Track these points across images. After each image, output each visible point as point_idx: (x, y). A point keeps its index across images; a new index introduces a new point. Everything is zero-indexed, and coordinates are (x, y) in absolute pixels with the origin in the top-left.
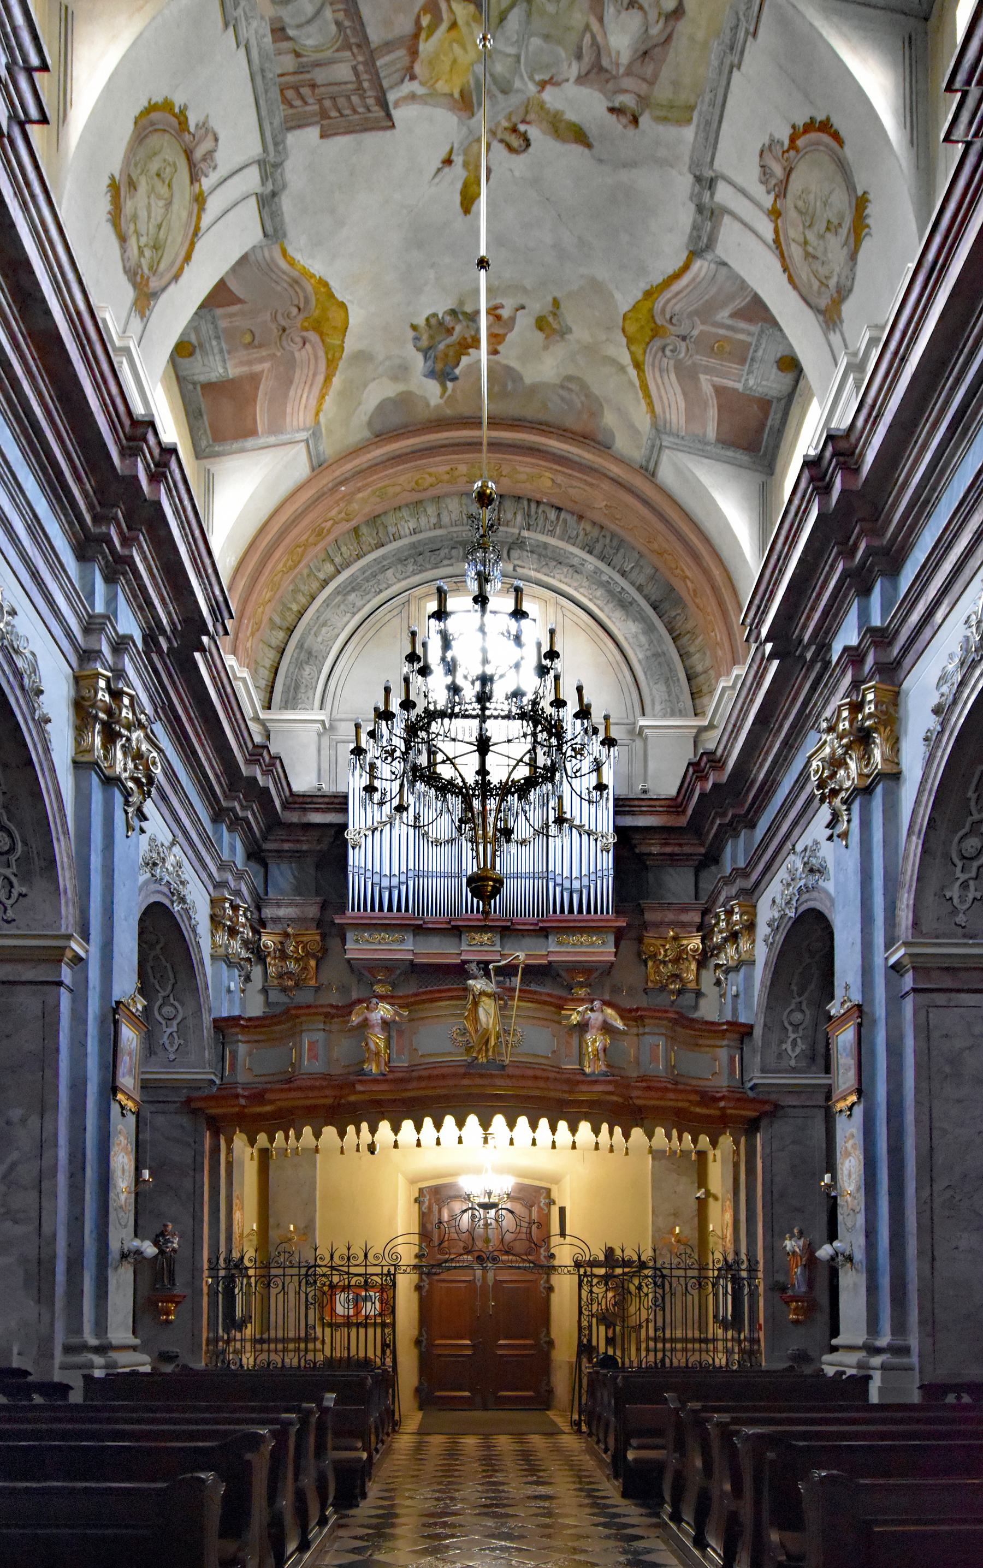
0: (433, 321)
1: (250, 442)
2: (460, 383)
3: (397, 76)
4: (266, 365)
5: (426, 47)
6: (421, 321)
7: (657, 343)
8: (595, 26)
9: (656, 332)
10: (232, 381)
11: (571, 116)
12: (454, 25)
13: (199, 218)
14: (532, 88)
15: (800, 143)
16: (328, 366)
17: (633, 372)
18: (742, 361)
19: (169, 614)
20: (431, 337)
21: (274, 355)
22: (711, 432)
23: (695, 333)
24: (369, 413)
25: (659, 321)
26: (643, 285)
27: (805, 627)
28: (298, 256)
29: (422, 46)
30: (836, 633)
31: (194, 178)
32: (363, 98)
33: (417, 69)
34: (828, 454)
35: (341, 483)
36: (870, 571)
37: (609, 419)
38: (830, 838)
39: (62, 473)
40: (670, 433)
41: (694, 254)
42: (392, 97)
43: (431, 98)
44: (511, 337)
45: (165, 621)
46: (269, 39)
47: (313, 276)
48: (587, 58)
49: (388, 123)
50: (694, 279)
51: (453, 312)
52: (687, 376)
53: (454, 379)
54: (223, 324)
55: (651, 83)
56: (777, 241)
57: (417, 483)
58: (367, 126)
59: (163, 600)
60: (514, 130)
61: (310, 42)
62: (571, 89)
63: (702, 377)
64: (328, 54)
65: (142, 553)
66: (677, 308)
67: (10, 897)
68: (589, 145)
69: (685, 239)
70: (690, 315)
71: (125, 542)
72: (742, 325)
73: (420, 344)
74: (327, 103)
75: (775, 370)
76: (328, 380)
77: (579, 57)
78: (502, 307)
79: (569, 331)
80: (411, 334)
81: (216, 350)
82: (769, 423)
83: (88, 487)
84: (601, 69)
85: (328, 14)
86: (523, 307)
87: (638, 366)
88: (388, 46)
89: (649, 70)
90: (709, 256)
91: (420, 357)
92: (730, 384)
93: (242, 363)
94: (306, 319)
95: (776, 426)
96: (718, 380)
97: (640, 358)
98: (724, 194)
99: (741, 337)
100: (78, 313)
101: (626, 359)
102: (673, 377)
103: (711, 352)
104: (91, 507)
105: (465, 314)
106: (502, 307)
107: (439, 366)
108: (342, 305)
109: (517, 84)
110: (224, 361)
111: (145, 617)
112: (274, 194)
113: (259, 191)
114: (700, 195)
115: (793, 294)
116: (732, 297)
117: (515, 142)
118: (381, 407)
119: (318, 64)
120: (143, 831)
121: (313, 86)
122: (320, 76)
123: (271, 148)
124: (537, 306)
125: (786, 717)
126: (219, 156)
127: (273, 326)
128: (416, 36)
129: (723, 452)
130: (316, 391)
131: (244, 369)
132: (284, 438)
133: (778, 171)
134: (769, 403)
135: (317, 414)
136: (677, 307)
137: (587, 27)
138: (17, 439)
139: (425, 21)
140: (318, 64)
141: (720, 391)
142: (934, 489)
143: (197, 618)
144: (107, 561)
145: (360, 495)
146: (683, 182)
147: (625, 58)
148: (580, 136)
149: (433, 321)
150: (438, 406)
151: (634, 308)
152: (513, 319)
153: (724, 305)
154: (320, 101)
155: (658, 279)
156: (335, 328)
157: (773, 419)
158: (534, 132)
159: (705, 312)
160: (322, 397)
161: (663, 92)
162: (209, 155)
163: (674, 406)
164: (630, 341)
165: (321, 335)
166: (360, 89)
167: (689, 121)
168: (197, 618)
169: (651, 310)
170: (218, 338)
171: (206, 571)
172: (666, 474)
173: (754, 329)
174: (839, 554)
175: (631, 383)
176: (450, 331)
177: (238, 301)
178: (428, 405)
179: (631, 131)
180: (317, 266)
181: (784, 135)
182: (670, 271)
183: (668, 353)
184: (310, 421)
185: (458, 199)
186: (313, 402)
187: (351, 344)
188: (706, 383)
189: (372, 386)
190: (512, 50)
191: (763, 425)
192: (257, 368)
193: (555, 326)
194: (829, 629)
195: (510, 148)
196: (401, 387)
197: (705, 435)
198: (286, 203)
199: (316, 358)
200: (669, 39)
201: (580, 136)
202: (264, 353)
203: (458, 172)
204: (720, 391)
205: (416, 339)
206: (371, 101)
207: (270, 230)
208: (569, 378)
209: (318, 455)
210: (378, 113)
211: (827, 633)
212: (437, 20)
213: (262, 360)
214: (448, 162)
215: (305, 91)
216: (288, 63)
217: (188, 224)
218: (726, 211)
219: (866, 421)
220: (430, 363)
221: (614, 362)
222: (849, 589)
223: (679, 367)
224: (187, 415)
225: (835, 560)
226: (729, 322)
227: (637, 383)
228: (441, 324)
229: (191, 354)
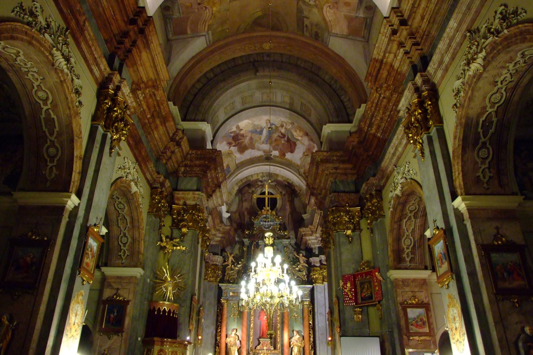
38: (415, 157)
67: (124, 256)
120: (119, 155)
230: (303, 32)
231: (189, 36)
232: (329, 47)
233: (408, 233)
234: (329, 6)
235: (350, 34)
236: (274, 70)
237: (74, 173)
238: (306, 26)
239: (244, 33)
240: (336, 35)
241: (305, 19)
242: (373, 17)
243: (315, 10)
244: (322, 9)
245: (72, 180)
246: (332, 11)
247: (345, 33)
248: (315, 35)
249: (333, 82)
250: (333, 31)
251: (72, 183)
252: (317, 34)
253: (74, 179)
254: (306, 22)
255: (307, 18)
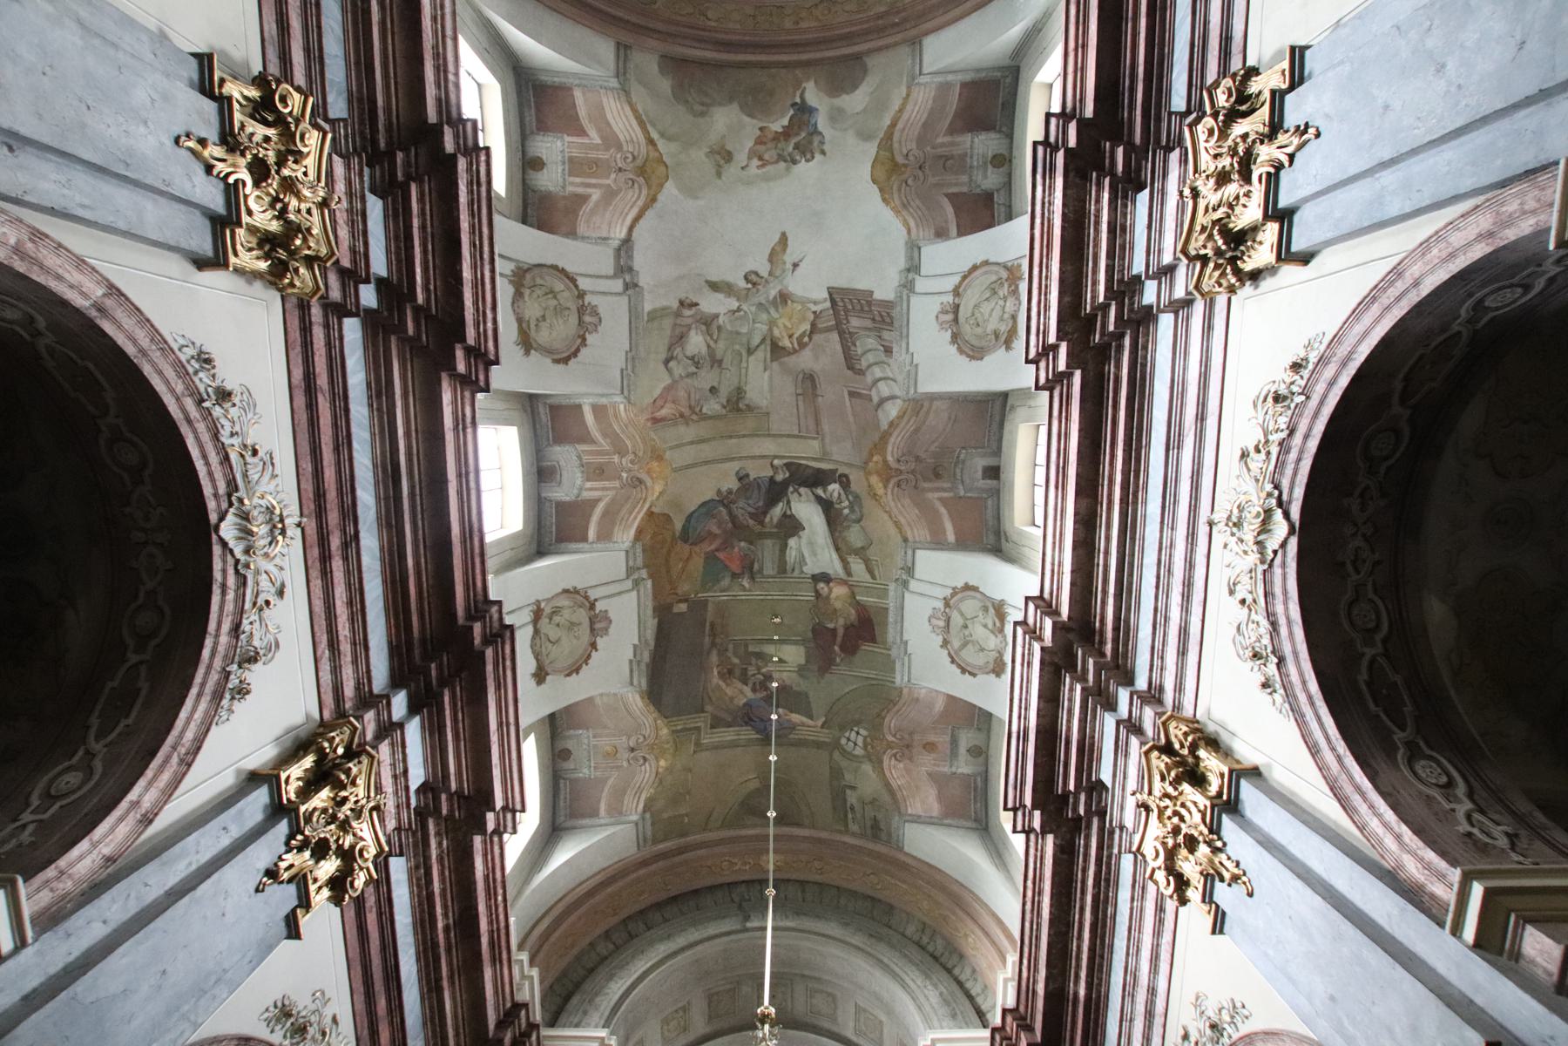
0: (808, 156)
1: (968, 77)
2: (790, 102)
3: (824, 314)
4: (940, 140)
5: (806, 327)
6: (818, 157)
7: (639, 162)
8: (712, 343)
9: (642, 171)
10: (970, 130)
11: (720, 296)
12: (790, 337)
13: (961, 283)
14: (745, 307)
15: (579, 341)
16: (892, 134)
17: (655, 135)
18: (571, 160)
19: (1098, 201)
20: (810, 143)
21: (933, 148)
22: (578, 94)
23: (613, 176)
24: (865, 83)
25: (641, 180)
26: (658, 205)
27: (421, 200)
28: (900, 226)
29: (808, 327)
30: (386, 216)
31: (956, 308)
32: (845, 306)
33: (812, 317)
34: (482, 377)
35: (897, 24)
36: (390, 310)
37: (665, 85)
39: (1128, 399)
40: (612, 89)
41: (627, 242)
42: (828, 304)
43: (804, 302)
44: (750, 144)
45: (1106, 196)
46: (894, 350)
47: (892, 209)
48: (714, 327)
49: (832, 292)
50: (624, 220)
51: (794, 162)
52: (611, 141)
53: (794, 105)
54: (965, 178)
55: (675, 325)
56: (573, 281)
57: (830, 11)
58: (844, 292)
59: (1097, 223)
60: (754, 284)
61: (870, 340)
62: (722, 310)
63: (598, 141)
64: (862, 332)
65: (1094, 291)
66: (631, 193)
68: (707, 282)
69: (636, 247)
70: (620, 190)
71: (1105, 308)
72: (580, 190)
73: (819, 138)
74: (866, 309)
75: (544, 158)
76: (893, 125)
77: (719, 328)
78: (758, 167)
79: (707, 155)
80: (826, 148)
81: (975, 158)
82: (533, 111)
83: (1112, 369)
84: (705, 324)
85: (860, 351)
86: (743, 168)
87: (651, 142)
88: (828, 330)
89: (678, 331)
90: (616, 243)
91: (820, 127)
92: (574, 139)
93: (958, 144)
94: (903, 173)
95: (526, 109)
96: (586, 141)
97: (650, 147)
98: (617, 285)
99: (578, 180)
100: (1057, 488)
101: (661, 144)
102: (621, 137)
103: (596, 163)
104: (1120, 348)
105: (785, 161)
106: (758, 167)
107: (806, 117)
108: (874, 181)
109: (753, 309)
110: (972, 147)
111: (1124, 215)
112: (908, 270)
113: (917, 277)
114: (632, 278)
115: (549, 262)
116: (593, 212)
117: (753, 277)
118: (855, 87)
119: (869, 329)
121: (873, 319)
122: (868, 323)
123: (905, 297)
124: (732, 170)
125: (383, 23)
126: (937, 308)
127: (927, 171)
128: (811, 332)
129: (563, 80)
130: (905, 116)
131: (959, 139)
132: (939, 79)
133: (587, 319)
134: (539, 129)
135: (908, 95)
136: (631, 195)
137: (716, 342)
138: (1145, 502)
139: (806, 339)
140: (869, 329)
141: (582, 132)
142: (379, 410)
143: (1072, 175)
144: (1131, 298)
145: (883, 9)
146: (644, 280)
147: (693, 333)
148: (714, 286)
149: (808, 156)
150: (808, 80)
151: (661, 186)
152: (750, 158)
153: (597, 204)
154: (871, 311)
155: (649, 213)
156: (883, 164)
157: (531, 117)
158: (742, 284)
159: (610, 195)
160: (901, 111)
161: (667, 323)
162: (944, 312)
163: (616, 113)
164: (660, 161)
165: (893, 159)
166: (846, 311)
167: (649, 313)
168: (1072, 175)
169: (649, 187)
170: (971, 167)
171: (1042, 224)
172: (605, 49)
173: (570, 189)
174: (429, 308)
175: (653, 125)
176: (797, 147)
177: (947, 195)
178: (816, 82)
179: (683, 296)
180: (887, 214)
181: (590, 338)
182: (641, 222)
183: (630, 156)
184: (915, 90)
185: (789, 243)
186: (909, 107)
187: (872, 149)
188: (595, 137)
189: (860, 108)
190: (757, 325)
191: (538, 110)
192: (948, 139)
193: (718, 157)
194: (396, 216)
195: (756, 274)
196: (838, 102)
197: (584, 94)
198: (902, 263)
199: (900, 142)
200: (669, 349)
201: (714, 286)
202: (940, 151)
203: (789, 258)
204: (582, 132)
205: (822, 143)
206: (841, 304)
207: (916, 250)
208: (702, 114)
209: (913, 51)
210: (837, 298)
211: (395, 210)
212: (800, 340)
213: (943, 145)
214: (795, 265)
215: (878, 318)
216: (886, 335)
217: (969, 286)
218: (615, 276)
219: (464, 415)
220: (813, 122)
221: (669, 138)
222: (400, 280)
223: (619, 147)
224: (1014, 108)
225: (428, 300)
226: (589, 190)
227: (650, 129)
228: (803, 154)
229: (994, 157)
230: (846, 825)
231: (602, 821)
232: (906, 849)
233: (1355, 577)
234: (895, 755)
235: (946, 815)
236: (787, 917)
237: (84, 845)
238: (852, 808)
239: (722, 827)
240: (917, 819)
241: (848, 792)
242: (987, 771)
243: (867, 768)
244: (881, 762)
245: (62, 863)
246: (901, 765)
247: (935, 813)
248: (872, 827)
249: (925, 940)
250: (910, 811)
251: (50, 872)
252: (875, 826)
253: (71, 865)
254: (852, 798)
255: (853, 788)
